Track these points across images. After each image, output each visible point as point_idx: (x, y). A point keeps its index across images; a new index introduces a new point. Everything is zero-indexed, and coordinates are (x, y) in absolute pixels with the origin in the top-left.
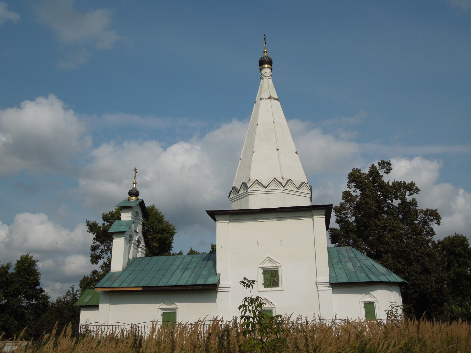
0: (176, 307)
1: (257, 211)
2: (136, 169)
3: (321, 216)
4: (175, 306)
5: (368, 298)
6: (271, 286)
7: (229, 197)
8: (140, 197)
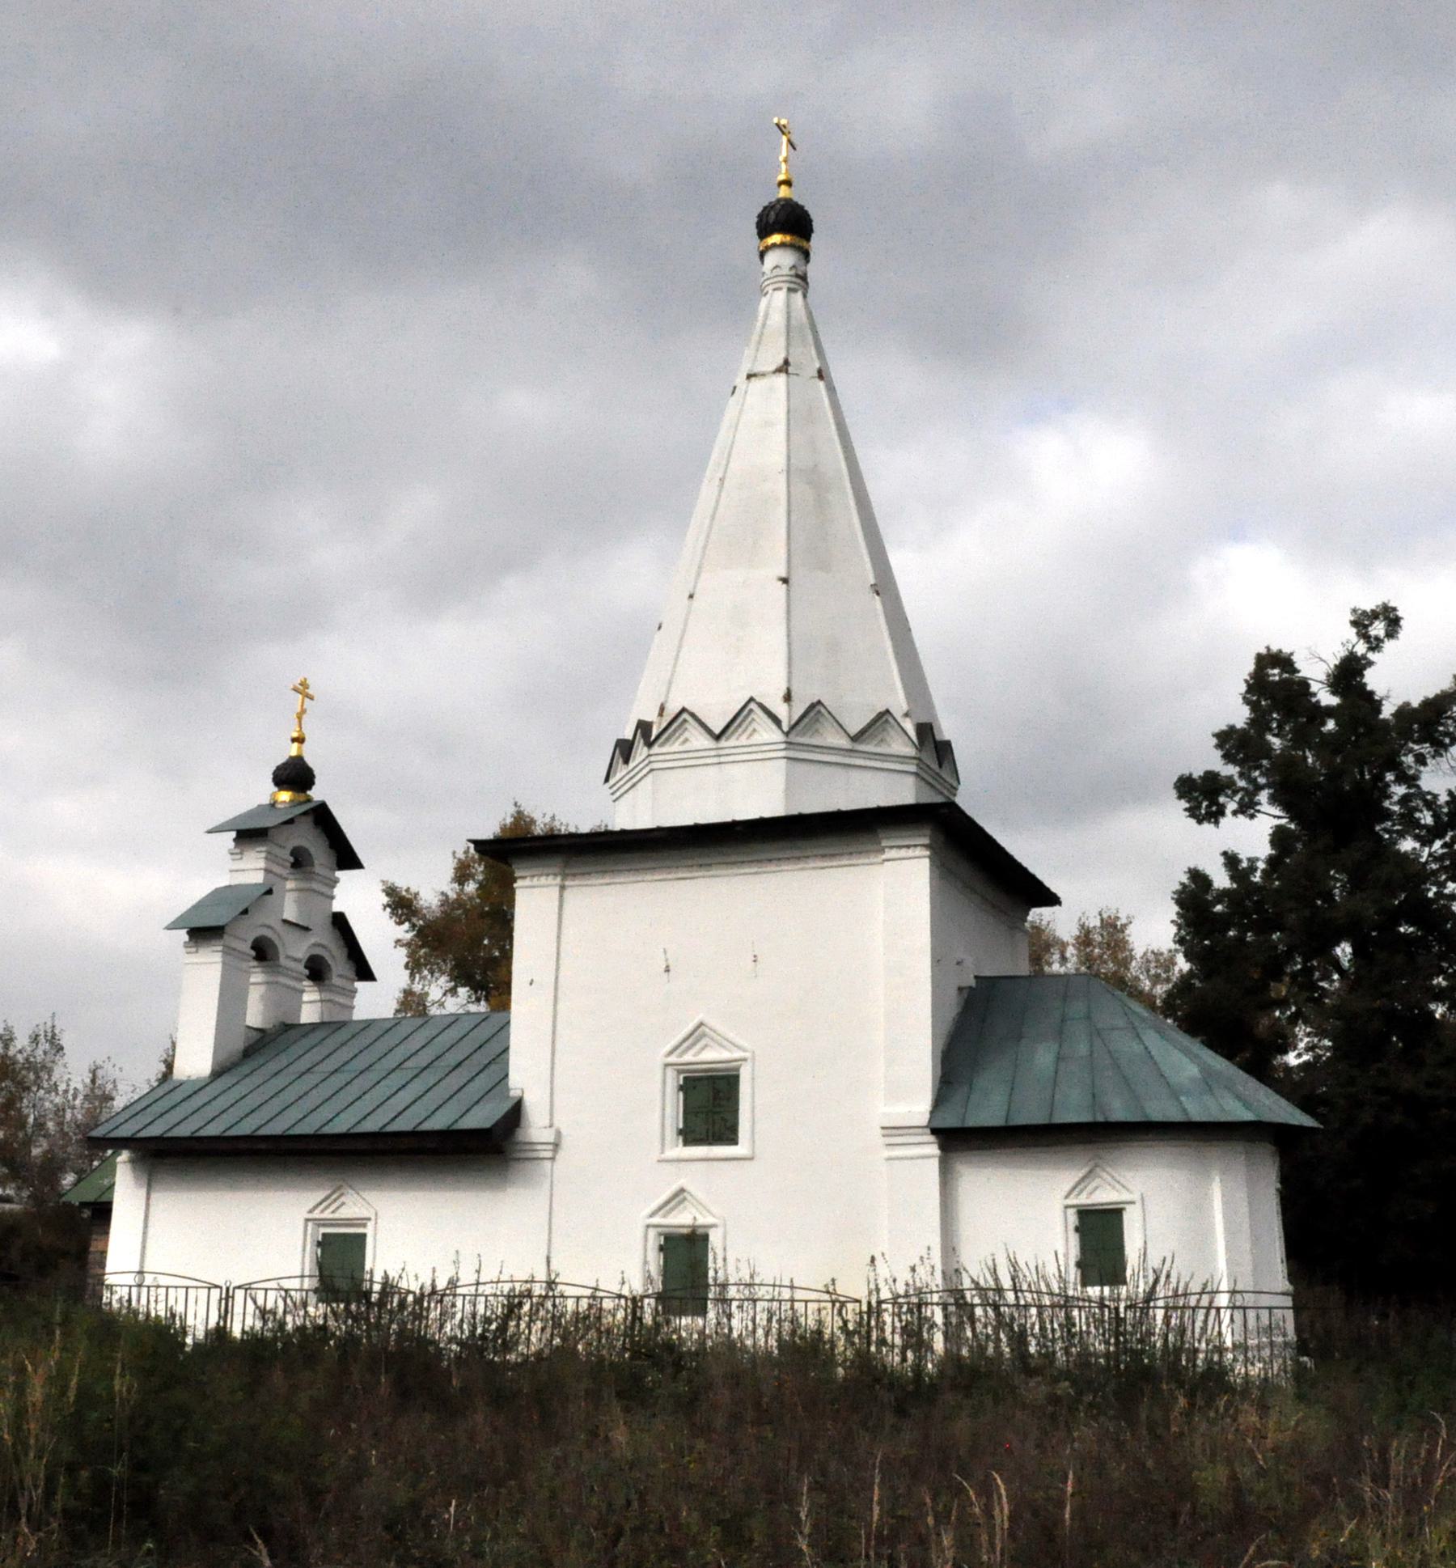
0: (364, 1213)
1: (602, 839)
2: (304, 684)
3: (910, 852)
4: (705, 1217)
5: (1103, 1195)
6: (710, 1138)
7: (607, 780)
8: (317, 794)
